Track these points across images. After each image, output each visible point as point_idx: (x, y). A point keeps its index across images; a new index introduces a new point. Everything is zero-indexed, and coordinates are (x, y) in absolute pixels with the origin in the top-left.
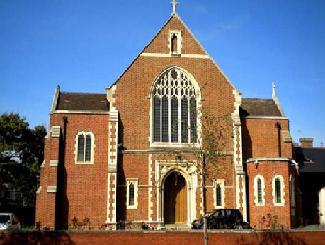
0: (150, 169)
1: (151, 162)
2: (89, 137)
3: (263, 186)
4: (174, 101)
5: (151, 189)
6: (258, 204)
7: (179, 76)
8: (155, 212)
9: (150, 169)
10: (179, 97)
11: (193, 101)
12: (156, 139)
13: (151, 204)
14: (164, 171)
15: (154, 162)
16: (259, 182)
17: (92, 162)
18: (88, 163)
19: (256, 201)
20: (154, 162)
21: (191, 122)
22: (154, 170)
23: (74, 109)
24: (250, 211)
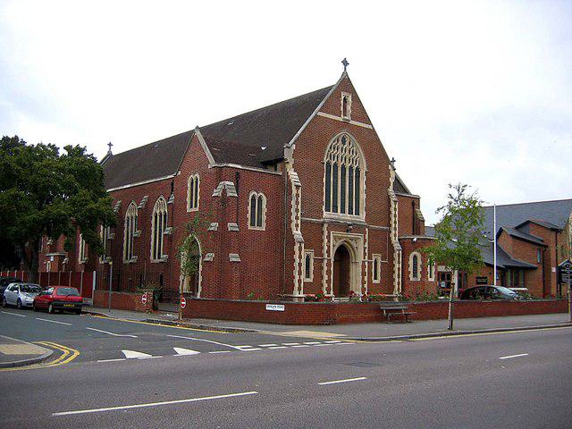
0: (326, 240)
1: (326, 233)
2: (260, 198)
3: (420, 262)
4: (343, 168)
5: (326, 261)
6: (430, 280)
7: (347, 143)
8: (329, 286)
9: (326, 240)
10: (348, 165)
11: (358, 171)
12: (328, 210)
13: (326, 277)
14: (338, 245)
15: (329, 233)
16: (415, 257)
17: (263, 228)
18: (258, 229)
19: (411, 276)
20: (329, 233)
21: (345, 181)
22: (329, 241)
23: (248, 165)
24: (524, 243)
